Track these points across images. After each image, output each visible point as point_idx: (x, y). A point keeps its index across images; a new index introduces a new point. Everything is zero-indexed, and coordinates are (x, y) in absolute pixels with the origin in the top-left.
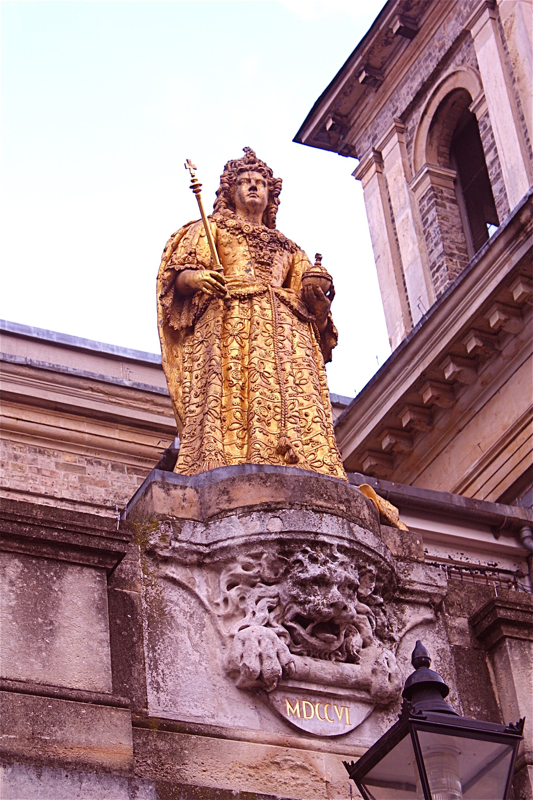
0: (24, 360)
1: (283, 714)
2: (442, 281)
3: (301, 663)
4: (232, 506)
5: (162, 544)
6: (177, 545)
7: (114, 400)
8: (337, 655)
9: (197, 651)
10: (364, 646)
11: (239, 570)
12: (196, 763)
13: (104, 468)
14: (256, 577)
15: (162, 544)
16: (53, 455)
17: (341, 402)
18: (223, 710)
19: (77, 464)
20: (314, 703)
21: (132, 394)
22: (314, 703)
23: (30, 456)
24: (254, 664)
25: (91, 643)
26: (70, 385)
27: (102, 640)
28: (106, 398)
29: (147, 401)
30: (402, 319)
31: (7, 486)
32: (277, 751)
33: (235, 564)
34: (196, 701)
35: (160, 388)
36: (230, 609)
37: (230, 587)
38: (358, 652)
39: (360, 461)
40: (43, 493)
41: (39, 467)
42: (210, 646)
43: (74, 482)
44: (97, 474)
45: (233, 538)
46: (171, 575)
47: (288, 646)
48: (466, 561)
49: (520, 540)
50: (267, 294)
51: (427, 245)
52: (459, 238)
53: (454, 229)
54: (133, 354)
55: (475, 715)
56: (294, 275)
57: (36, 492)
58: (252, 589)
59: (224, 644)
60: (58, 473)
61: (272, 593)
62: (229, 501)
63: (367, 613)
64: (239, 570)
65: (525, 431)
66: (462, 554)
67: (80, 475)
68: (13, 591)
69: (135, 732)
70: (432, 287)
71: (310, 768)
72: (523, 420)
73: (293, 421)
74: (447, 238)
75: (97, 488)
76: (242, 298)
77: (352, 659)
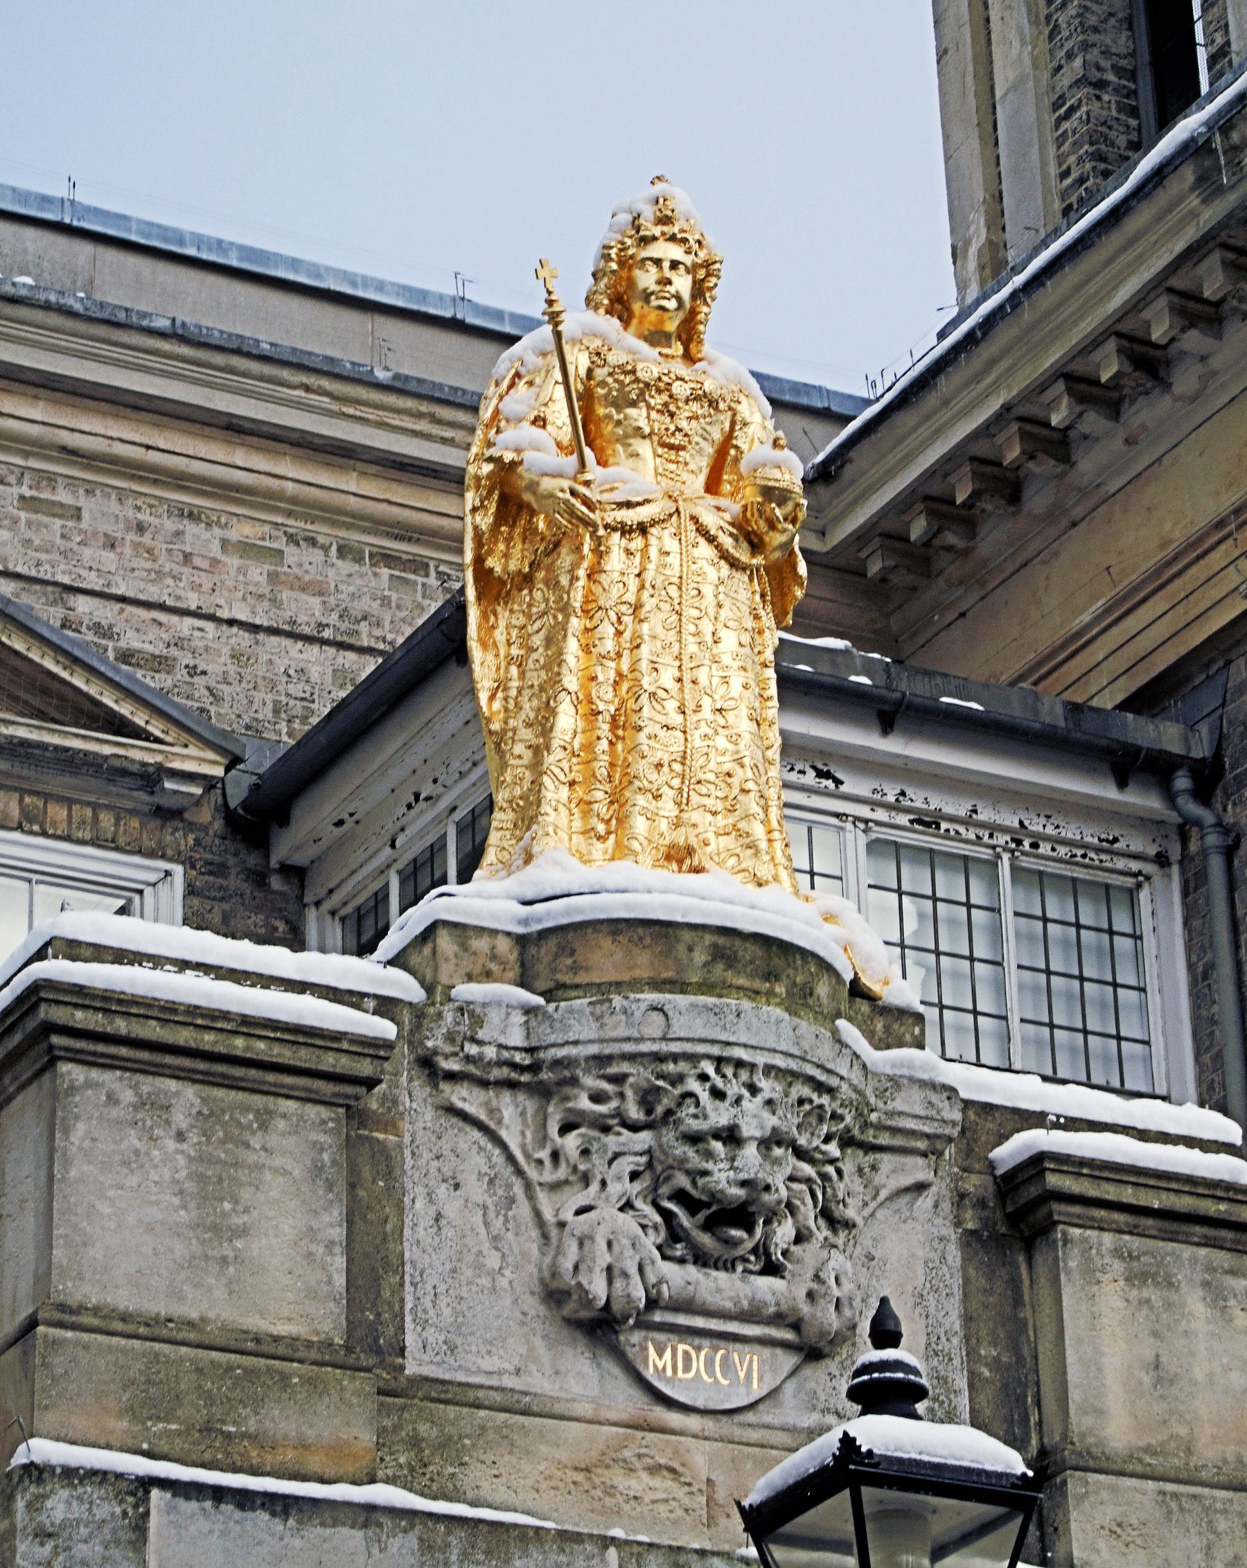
0: (168, 323)
1: (641, 1369)
2: (1074, 143)
3: (677, 1277)
4: (577, 980)
5: (448, 1049)
6: (472, 1049)
7: (351, 411)
8: (747, 1261)
9: (496, 1248)
10: (799, 1239)
11: (584, 1103)
12: (483, 1462)
13: (321, 552)
14: (612, 1117)
15: (448, 1049)
16: (218, 523)
17: (833, 408)
18: (535, 1360)
19: (267, 544)
20: (698, 1349)
21: (391, 399)
22: (698, 1349)
23: (170, 525)
24: (598, 1289)
25: (313, 1248)
26: (261, 378)
27: (332, 1243)
28: (335, 407)
29: (420, 415)
30: (982, 209)
31: (119, 592)
32: (626, 1439)
33: (575, 1091)
34: (490, 1343)
35: (451, 387)
36: (562, 1173)
37: (566, 1129)
38: (785, 1253)
39: (863, 554)
40: (193, 607)
41: (188, 550)
42: (522, 1239)
43: (257, 584)
44: (306, 566)
45: (576, 1043)
46: (459, 1104)
47: (659, 1248)
48: (1055, 832)
49: (1170, 797)
50: (675, 518)
51: (1051, 51)
52: (1120, 42)
53: (1112, 21)
54: (398, 294)
55: (987, 1365)
56: (733, 452)
57: (179, 604)
58: (602, 1136)
59: (545, 1236)
60: (225, 564)
61: (639, 1148)
62: (575, 968)
63: (808, 1181)
64: (584, 1103)
65: (1202, 562)
66: (1048, 817)
67: (272, 568)
68: (183, 1152)
69: (382, 1409)
70: (1052, 151)
71: (680, 1469)
72: (1201, 539)
73: (704, 791)
74: (1094, 45)
75: (305, 597)
76: (625, 530)
77: (772, 1269)
